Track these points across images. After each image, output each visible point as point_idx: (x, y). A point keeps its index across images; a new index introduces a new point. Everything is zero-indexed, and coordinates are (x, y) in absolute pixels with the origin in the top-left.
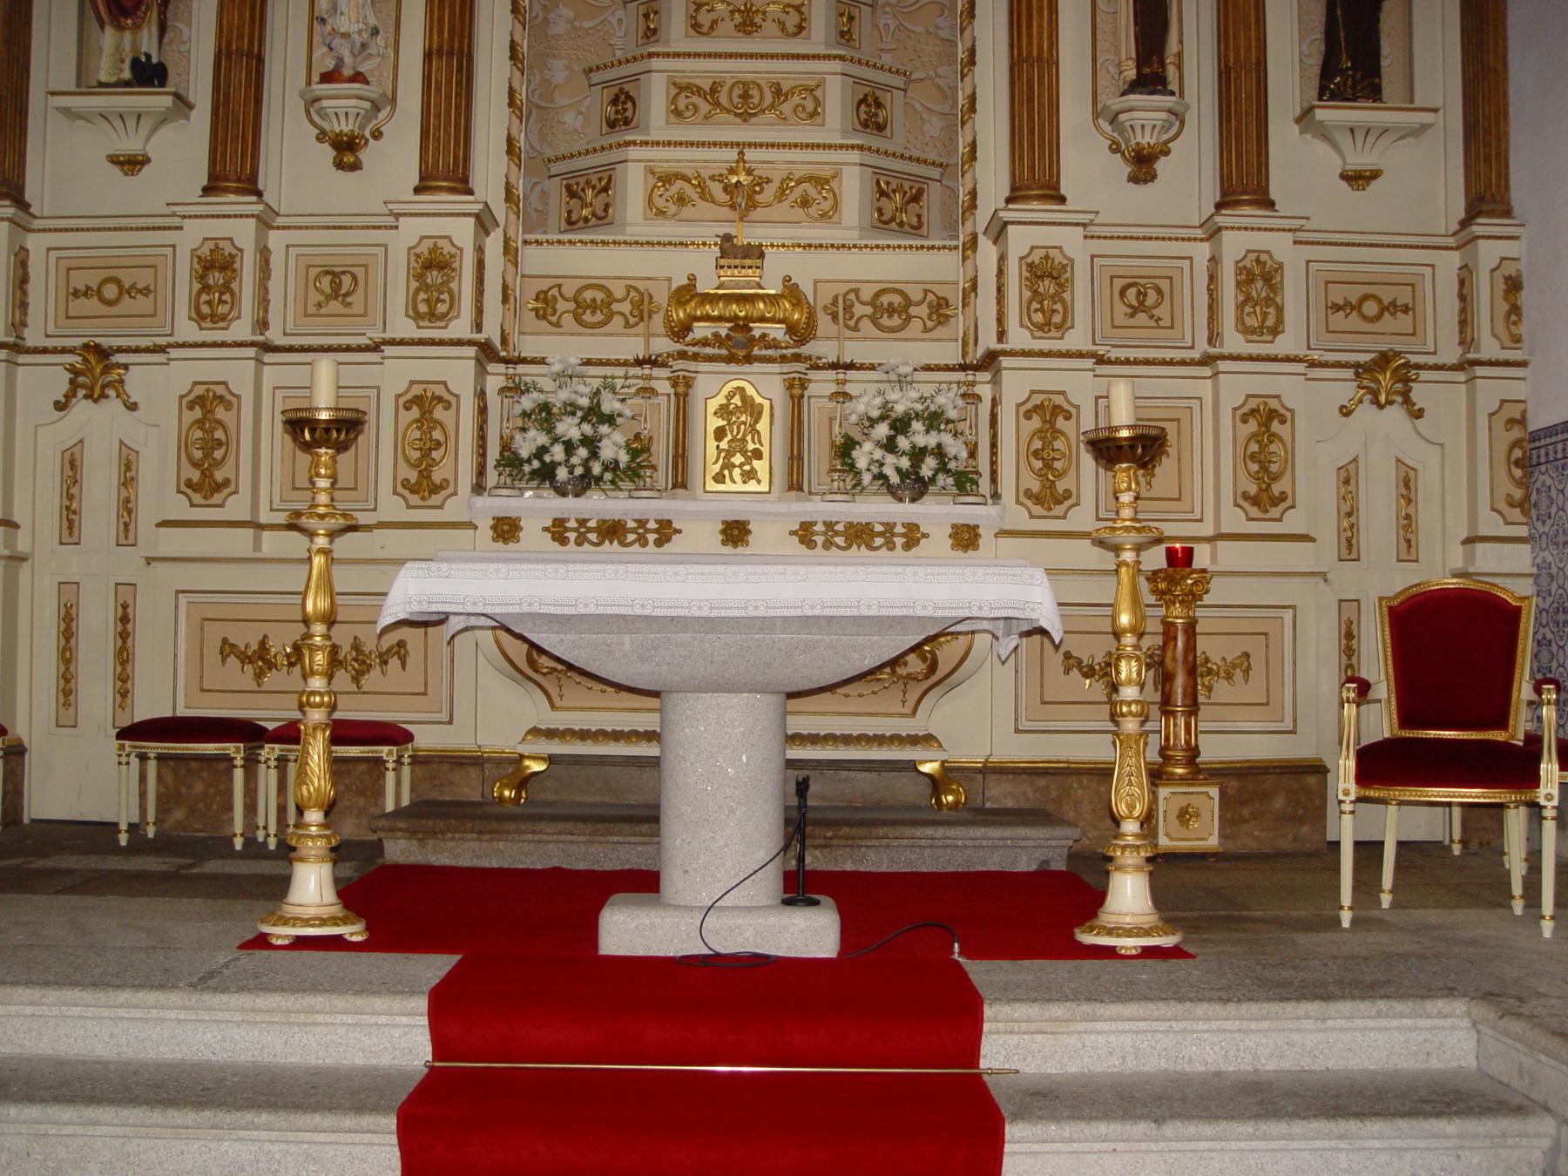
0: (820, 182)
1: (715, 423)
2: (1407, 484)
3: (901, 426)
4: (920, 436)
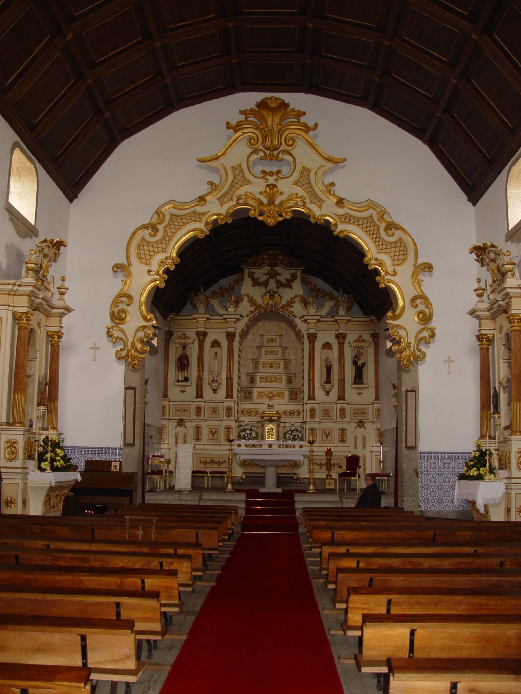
0: (282, 393)
1: (267, 431)
2: (364, 438)
3: (292, 431)
4: (295, 433)
